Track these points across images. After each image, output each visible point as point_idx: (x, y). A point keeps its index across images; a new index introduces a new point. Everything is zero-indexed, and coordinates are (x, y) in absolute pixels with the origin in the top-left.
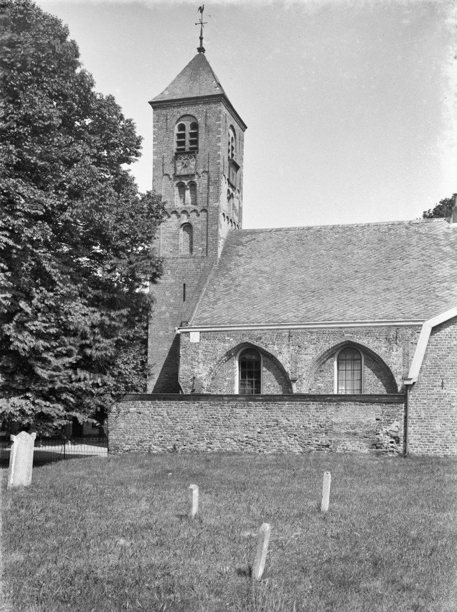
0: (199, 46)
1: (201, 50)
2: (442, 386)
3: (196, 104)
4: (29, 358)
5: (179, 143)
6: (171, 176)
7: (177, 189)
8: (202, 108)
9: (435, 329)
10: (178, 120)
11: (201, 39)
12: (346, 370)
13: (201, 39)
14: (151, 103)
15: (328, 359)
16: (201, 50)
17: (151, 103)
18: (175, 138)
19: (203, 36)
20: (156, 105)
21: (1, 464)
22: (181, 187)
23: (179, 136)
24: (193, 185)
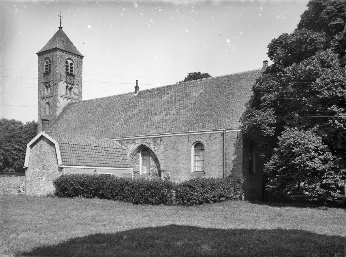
0: (59, 26)
1: (60, 28)
2: (34, 169)
3: (49, 53)
4: (313, 150)
5: (46, 69)
6: (43, 83)
7: (46, 88)
8: (51, 54)
9: (32, 146)
10: (45, 60)
11: (61, 23)
12: (148, 159)
13: (61, 23)
14: (37, 54)
15: (134, 156)
16: (60, 28)
17: (37, 54)
18: (45, 67)
19: (60, 24)
20: (39, 54)
21: (342, 239)
22: (46, 86)
23: (46, 66)
24: (50, 85)
